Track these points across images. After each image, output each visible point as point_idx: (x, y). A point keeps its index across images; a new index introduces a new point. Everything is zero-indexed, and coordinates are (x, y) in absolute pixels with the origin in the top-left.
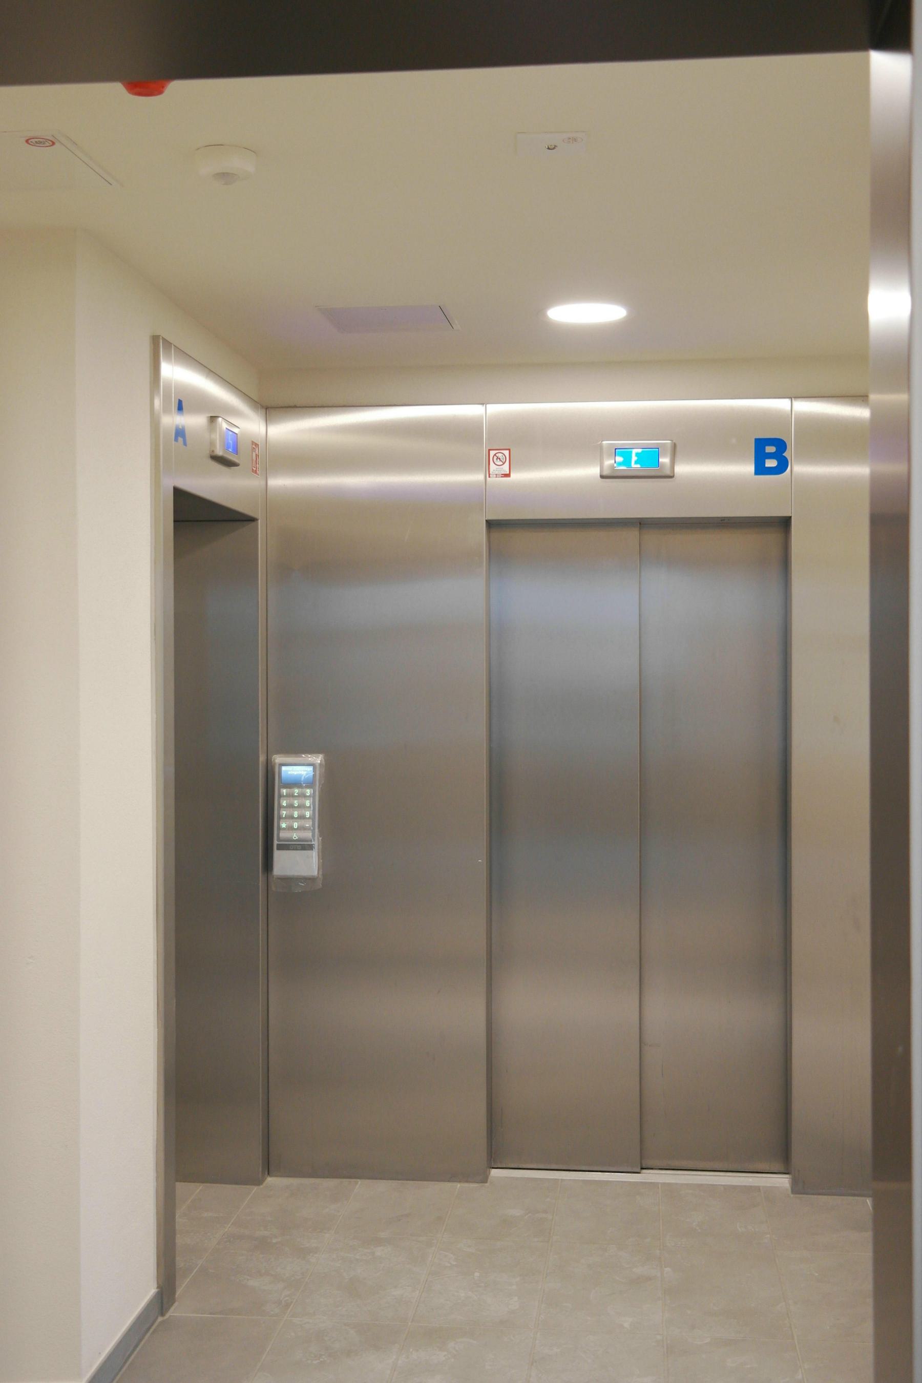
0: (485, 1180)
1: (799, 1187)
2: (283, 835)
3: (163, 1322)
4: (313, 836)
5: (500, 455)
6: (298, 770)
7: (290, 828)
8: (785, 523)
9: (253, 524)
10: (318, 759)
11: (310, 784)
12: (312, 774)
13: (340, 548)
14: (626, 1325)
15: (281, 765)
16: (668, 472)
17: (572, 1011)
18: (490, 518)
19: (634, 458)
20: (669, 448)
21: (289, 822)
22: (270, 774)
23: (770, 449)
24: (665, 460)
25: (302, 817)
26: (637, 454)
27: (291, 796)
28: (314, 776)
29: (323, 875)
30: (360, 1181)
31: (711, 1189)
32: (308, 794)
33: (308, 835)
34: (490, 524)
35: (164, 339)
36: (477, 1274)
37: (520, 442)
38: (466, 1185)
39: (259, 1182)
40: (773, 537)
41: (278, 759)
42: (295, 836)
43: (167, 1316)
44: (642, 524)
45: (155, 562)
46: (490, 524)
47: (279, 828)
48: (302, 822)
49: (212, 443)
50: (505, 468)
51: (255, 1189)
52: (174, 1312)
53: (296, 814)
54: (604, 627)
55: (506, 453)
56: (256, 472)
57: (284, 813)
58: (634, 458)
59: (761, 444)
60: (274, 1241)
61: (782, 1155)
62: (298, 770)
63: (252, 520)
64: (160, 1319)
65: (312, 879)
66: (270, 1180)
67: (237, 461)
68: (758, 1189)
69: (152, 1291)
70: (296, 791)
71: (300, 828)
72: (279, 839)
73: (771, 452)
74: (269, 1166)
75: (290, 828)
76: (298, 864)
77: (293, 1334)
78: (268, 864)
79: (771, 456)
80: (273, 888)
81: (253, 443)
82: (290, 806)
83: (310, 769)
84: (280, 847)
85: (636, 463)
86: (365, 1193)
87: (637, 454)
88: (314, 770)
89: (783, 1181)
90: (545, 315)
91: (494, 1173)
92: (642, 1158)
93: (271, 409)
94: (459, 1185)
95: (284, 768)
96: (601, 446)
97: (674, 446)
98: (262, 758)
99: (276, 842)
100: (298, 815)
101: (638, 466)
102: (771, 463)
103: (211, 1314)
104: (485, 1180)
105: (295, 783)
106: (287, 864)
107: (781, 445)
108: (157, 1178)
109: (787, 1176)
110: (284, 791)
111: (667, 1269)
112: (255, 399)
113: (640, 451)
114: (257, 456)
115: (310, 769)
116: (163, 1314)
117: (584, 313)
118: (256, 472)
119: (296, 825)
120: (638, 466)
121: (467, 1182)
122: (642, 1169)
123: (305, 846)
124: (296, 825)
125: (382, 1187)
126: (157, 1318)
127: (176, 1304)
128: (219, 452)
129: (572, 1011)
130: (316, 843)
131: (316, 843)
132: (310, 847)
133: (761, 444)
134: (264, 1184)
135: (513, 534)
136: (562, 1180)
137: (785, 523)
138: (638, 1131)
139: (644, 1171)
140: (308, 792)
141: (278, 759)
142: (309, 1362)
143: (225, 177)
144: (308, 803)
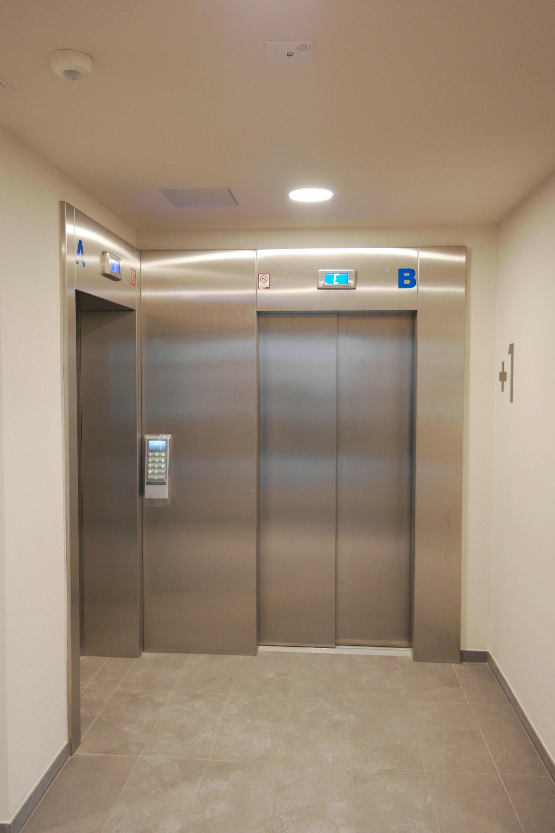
0: (255, 653)
1: (417, 657)
2: (149, 477)
3: (71, 759)
4: (166, 477)
5: (264, 277)
6: (158, 443)
7: (154, 473)
8: (413, 314)
9: (132, 313)
10: (168, 437)
11: (165, 450)
12: (165, 445)
13: (175, 325)
14: (330, 759)
15: (149, 440)
16: (353, 286)
17: (300, 553)
18: (259, 310)
19: (335, 279)
20: (354, 273)
21: (153, 470)
22: (143, 444)
23: (407, 275)
24: (351, 282)
25: (160, 468)
26: (337, 277)
27: (154, 456)
28: (166, 446)
29: (171, 497)
30: (191, 655)
31: (372, 658)
32: (163, 456)
33: (163, 477)
34: (259, 313)
35: (67, 203)
36: (249, 721)
37: (277, 272)
38: (245, 657)
39: (137, 656)
40: (406, 322)
41: (147, 437)
42: (156, 478)
43: (74, 755)
44: (338, 314)
45: (63, 333)
46: (259, 313)
47: (148, 473)
48: (160, 470)
49: (103, 267)
50: (267, 284)
51: (136, 660)
52: (79, 752)
53: (156, 466)
54: (317, 363)
55: (268, 275)
56: (134, 285)
57: (150, 465)
58: (335, 279)
59: (402, 272)
60: (141, 697)
61: (407, 634)
62: (158, 443)
63: (133, 310)
64: (70, 758)
65: (164, 500)
66: (144, 654)
67: (120, 278)
68: (395, 658)
69: (65, 742)
70: (157, 454)
71: (159, 473)
72: (148, 479)
73: (407, 276)
74: (143, 647)
75: (154, 473)
76: (158, 493)
77: (143, 769)
78: (142, 491)
79: (407, 278)
80: (145, 505)
81: (132, 269)
82: (154, 462)
83: (164, 442)
84: (148, 483)
85: (336, 281)
86: (195, 661)
87: (337, 277)
88: (166, 443)
89: (407, 653)
90: (288, 196)
91: (261, 648)
92: (336, 637)
93: (143, 253)
94: (242, 657)
95: (150, 442)
96: (317, 272)
97: (356, 273)
98: (138, 436)
99: (146, 481)
100: (158, 466)
101: (337, 283)
102: (407, 282)
103: (99, 753)
104: (255, 654)
105: (155, 450)
106: (151, 492)
107: (412, 272)
108: (68, 680)
109: (410, 649)
110: (150, 454)
111: (351, 716)
112: (134, 244)
113: (338, 275)
114: (134, 276)
115: (164, 442)
116: (71, 755)
117: (310, 195)
118: (134, 285)
119: (156, 472)
120: (337, 283)
121: (246, 655)
122: (336, 645)
123: (161, 483)
124: (156, 472)
125: (202, 658)
126: (68, 758)
127: (81, 746)
128: (108, 272)
129: (300, 553)
130: (167, 481)
131: (167, 481)
132: (164, 484)
133: (402, 272)
134: (141, 657)
135: (272, 319)
136: (296, 653)
137: (413, 314)
138: (333, 623)
139: (337, 647)
140: (163, 454)
141: (147, 437)
142: (150, 792)
143: (72, 74)
144: (163, 460)
